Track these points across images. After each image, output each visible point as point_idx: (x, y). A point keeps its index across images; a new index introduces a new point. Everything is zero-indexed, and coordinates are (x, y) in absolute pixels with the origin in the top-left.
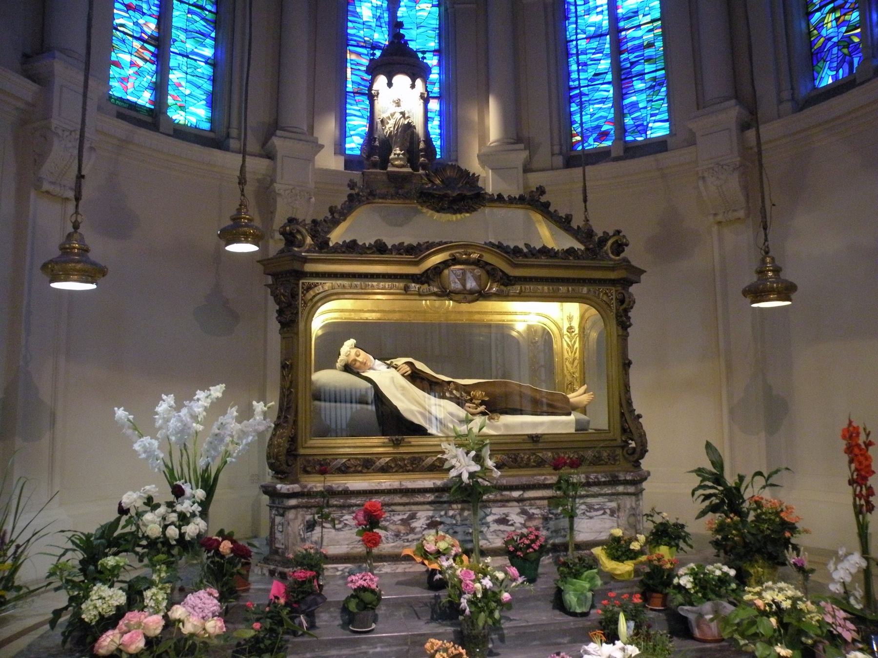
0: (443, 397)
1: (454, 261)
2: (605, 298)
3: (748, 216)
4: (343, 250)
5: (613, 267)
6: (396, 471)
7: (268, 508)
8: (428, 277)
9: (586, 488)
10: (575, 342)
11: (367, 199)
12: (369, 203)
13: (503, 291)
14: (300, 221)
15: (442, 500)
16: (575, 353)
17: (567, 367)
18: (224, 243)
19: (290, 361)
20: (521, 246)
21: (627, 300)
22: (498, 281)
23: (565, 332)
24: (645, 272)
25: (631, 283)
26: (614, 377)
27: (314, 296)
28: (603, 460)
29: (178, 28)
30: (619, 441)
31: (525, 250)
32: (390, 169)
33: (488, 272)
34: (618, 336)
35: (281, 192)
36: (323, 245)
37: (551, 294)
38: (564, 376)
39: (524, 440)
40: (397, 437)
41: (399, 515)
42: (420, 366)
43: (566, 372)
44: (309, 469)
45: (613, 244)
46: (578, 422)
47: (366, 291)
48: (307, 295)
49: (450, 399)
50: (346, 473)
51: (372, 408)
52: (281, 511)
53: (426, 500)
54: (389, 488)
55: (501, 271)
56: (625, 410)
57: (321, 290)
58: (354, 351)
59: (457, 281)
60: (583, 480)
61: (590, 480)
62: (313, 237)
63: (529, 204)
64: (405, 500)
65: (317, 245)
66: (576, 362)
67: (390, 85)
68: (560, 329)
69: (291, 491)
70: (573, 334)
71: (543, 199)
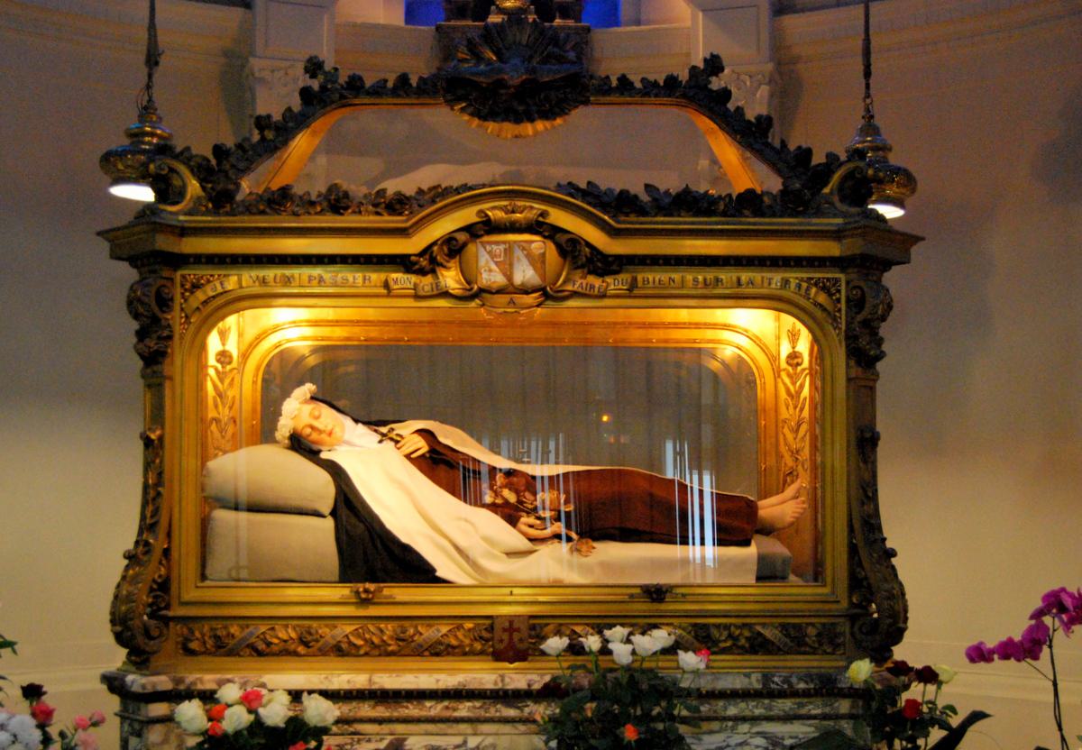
0: (478, 502)
1: (489, 227)
2: (822, 298)
4: (262, 207)
5: (838, 231)
6: (366, 654)
7: (118, 720)
8: (433, 261)
9: (766, 701)
10: (802, 386)
11: (342, 97)
12: (344, 106)
13: (592, 287)
14: (178, 150)
15: (456, 714)
16: (802, 410)
17: (785, 439)
18: (110, 180)
19: (158, 433)
20: (637, 189)
21: (869, 302)
22: (582, 267)
23: (783, 364)
24: (923, 239)
25: (887, 265)
26: (837, 464)
27: (205, 303)
28: (806, 644)
30: (844, 604)
31: (645, 198)
33: (559, 246)
34: (849, 380)
35: (266, 74)
37: (700, 292)
38: (779, 456)
39: (631, 596)
40: (368, 585)
41: (369, 741)
42: (452, 437)
43: (783, 449)
44: (194, 645)
45: (844, 179)
46: (762, 559)
47: (308, 291)
48: (191, 299)
49: (493, 507)
50: (267, 655)
52: (137, 726)
53: (424, 713)
54: (347, 687)
55: (588, 245)
56: (859, 540)
57: (220, 290)
58: (308, 408)
59: (493, 267)
60: (758, 686)
61: (773, 686)
62: (202, 181)
63: (684, 96)
64: (381, 711)
65: (210, 199)
66: (804, 427)
68: (773, 359)
69: (149, 689)
70: (799, 368)
71: (716, 84)
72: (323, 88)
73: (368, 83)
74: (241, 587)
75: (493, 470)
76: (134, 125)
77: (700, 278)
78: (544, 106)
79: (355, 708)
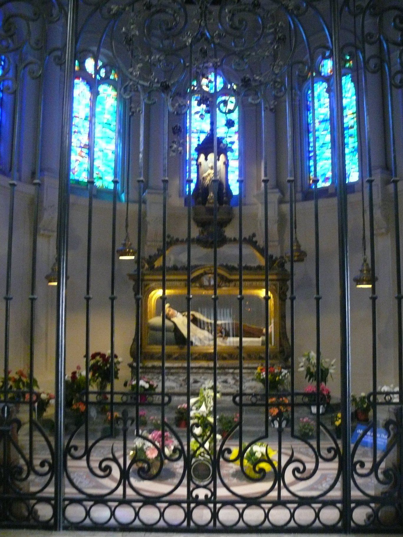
3: (387, 231)
29: (98, 138)
32: (207, 205)
36: (152, 267)
51: (173, 334)
62: (148, 264)
67: (206, 159)
71: (254, 239)
72: (171, 241)
73: (180, 239)
74: (295, 213)
75: (207, 323)
76: (123, 242)
77: (249, 283)
78: (282, 26)
79: (176, 379)
